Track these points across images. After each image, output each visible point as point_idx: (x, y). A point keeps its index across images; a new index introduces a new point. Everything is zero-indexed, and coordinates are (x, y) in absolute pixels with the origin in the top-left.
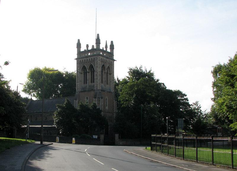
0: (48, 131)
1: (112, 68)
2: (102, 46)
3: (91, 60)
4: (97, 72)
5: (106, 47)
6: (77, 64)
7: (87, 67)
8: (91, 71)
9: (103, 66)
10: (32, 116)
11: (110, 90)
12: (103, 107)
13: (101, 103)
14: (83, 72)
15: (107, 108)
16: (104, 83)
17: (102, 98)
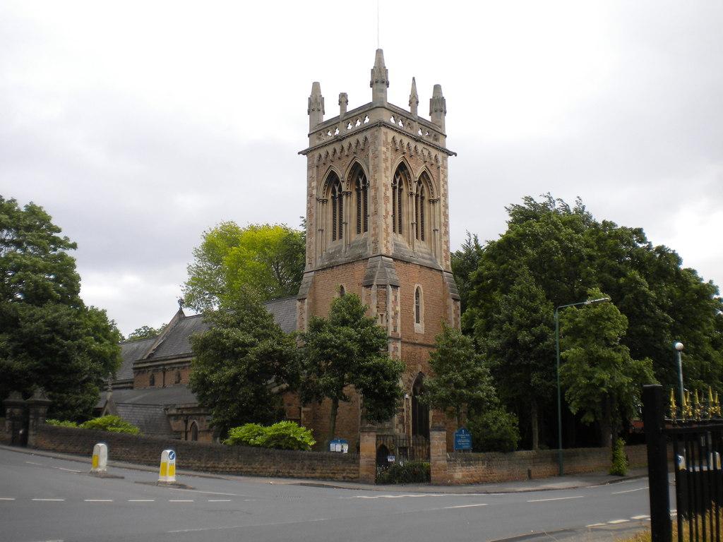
0: (186, 422)
2: (397, 96)
3: (353, 145)
4: (376, 189)
5: (414, 101)
6: (310, 168)
7: (342, 173)
8: (358, 190)
11: (431, 259)
12: (399, 321)
13: (390, 305)
14: (330, 197)
15: (419, 328)
16: (405, 231)
17: (395, 287)
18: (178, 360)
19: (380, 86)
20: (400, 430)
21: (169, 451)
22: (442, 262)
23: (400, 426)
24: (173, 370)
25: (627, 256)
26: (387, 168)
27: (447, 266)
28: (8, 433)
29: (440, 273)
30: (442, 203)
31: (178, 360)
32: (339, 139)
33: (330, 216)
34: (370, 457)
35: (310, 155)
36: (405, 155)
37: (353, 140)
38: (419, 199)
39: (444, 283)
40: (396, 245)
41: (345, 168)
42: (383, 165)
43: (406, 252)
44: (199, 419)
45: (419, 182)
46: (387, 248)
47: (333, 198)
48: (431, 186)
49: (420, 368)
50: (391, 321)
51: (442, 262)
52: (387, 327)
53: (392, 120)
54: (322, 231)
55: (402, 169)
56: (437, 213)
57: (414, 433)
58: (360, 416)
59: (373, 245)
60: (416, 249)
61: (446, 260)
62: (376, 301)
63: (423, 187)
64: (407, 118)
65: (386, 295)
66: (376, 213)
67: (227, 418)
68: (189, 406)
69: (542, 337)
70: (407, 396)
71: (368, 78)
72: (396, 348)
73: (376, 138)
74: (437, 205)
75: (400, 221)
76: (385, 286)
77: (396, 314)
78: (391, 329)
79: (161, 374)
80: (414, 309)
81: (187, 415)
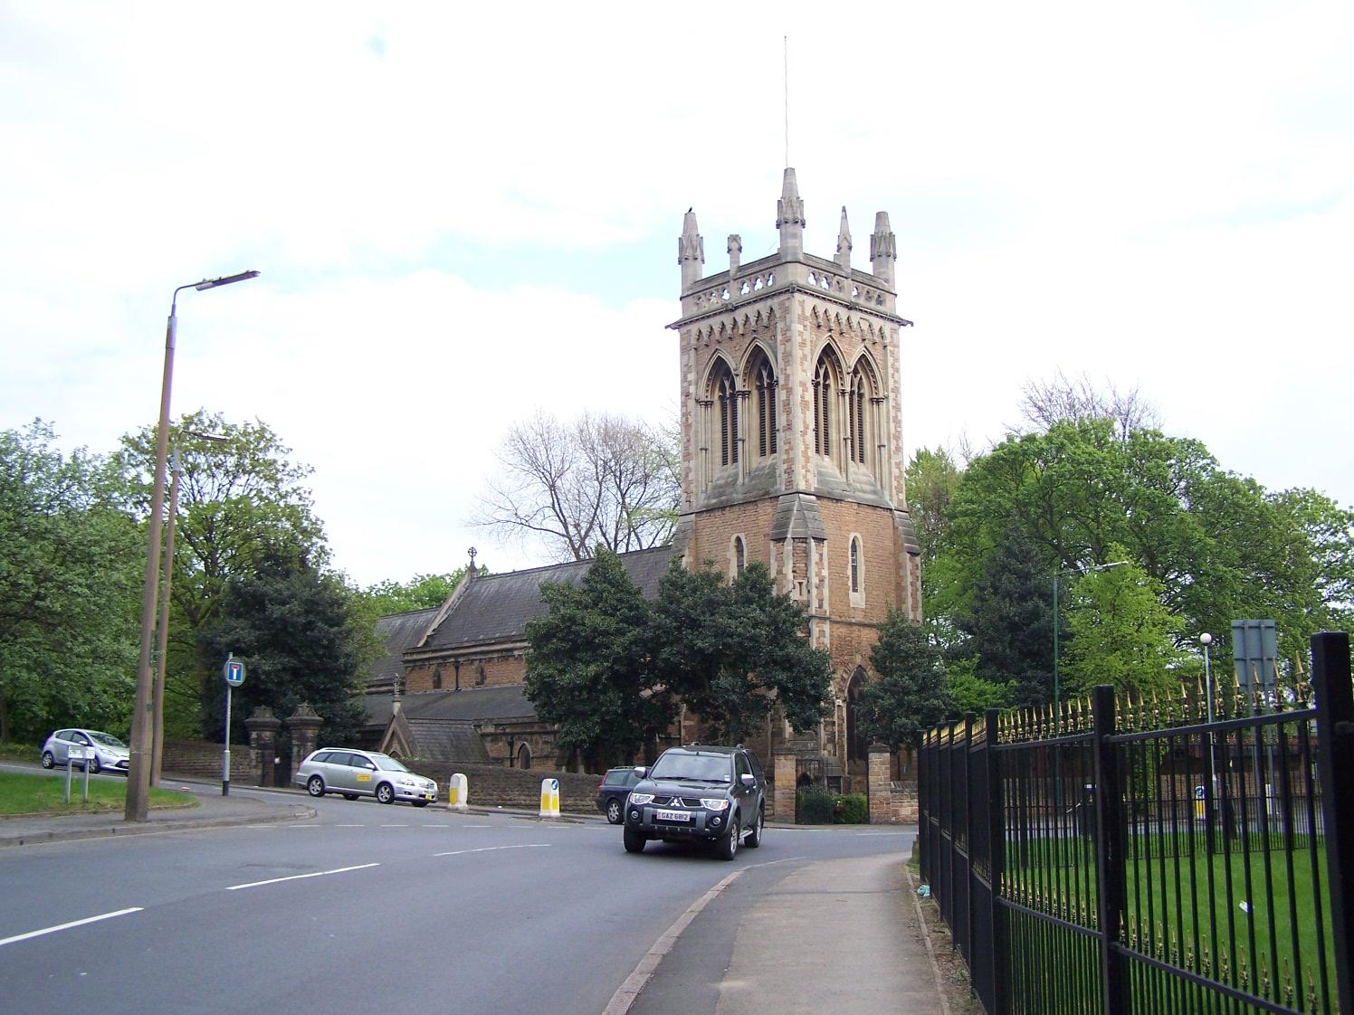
0: (511, 744)
1: (886, 368)
3: (753, 319)
4: (789, 391)
5: (845, 245)
6: (684, 350)
7: (736, 363)
8: (760, 388)
9: (828, 352)
10: (461, 660)
11: (875, 492)
12: (826, 592)
13: (813, 569)
15: (858, 599)
16: (834, 450)
17: (820, 540)
18: (478, 649)
19: (790, 228)
20: (829, 752)
21: (551, 780)
22: (891, 496)
23: (830, 747)
24: (472, 663)
25: (1125, 514)
26: (805, 356)
27: (900, 502)
28: (255, 767)
29: (888, 513)
30: (891, 403)
31: (478, 649)
32: (730, 309)
33: (718, 426)
34: (788, 787)
35: (684, 329)
36: (832, 333)
37: (751, 311)
38: (856, 397)
39: (895, 528)
40: (820, 474)
41: (739, 354)
42: (798, 353)
43: (837, 483)
44: (532, 740)
45: (856, 372)
46: (807, 481)
47: (722, 398)
48: (874, 376)
49: (858, 660)
50: (814, 591)
51: (891, 496)
52: (809, 601)
53: (811, 280)
54: (706, 450)
55: (828, 355)
56: (883, 420)
57: (850, 757)
58: (769, 733)
59: (785, 476)
60: (851, 478)
61: (899, 491)
62: (791, 562)
63: (861, 378)
64: (835, 275)
65: (807, 554)
66: (789, 427)
67: (583, 737)
68: (514, 721)
69: (1035, 615)
70: (839, 702)
71: (773, 216)
72: (822, 633)
73: (787, 310)
74: (883, 406)
75: (826, 434)
76: (804, 540)
77: (822, 581)
78: (815, 604)
79: (452, 669)
80: (850, 572)
81: (513, 735)
